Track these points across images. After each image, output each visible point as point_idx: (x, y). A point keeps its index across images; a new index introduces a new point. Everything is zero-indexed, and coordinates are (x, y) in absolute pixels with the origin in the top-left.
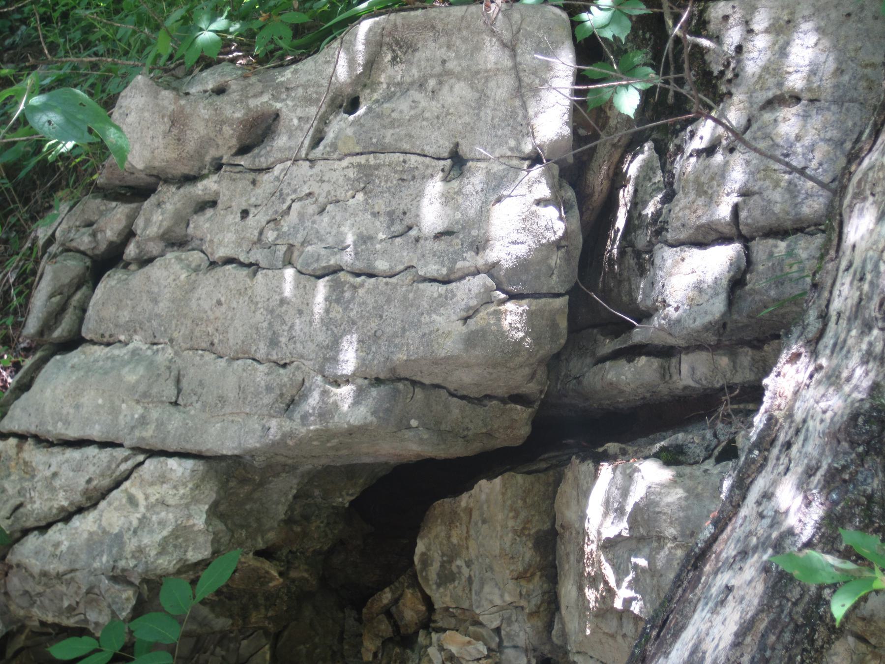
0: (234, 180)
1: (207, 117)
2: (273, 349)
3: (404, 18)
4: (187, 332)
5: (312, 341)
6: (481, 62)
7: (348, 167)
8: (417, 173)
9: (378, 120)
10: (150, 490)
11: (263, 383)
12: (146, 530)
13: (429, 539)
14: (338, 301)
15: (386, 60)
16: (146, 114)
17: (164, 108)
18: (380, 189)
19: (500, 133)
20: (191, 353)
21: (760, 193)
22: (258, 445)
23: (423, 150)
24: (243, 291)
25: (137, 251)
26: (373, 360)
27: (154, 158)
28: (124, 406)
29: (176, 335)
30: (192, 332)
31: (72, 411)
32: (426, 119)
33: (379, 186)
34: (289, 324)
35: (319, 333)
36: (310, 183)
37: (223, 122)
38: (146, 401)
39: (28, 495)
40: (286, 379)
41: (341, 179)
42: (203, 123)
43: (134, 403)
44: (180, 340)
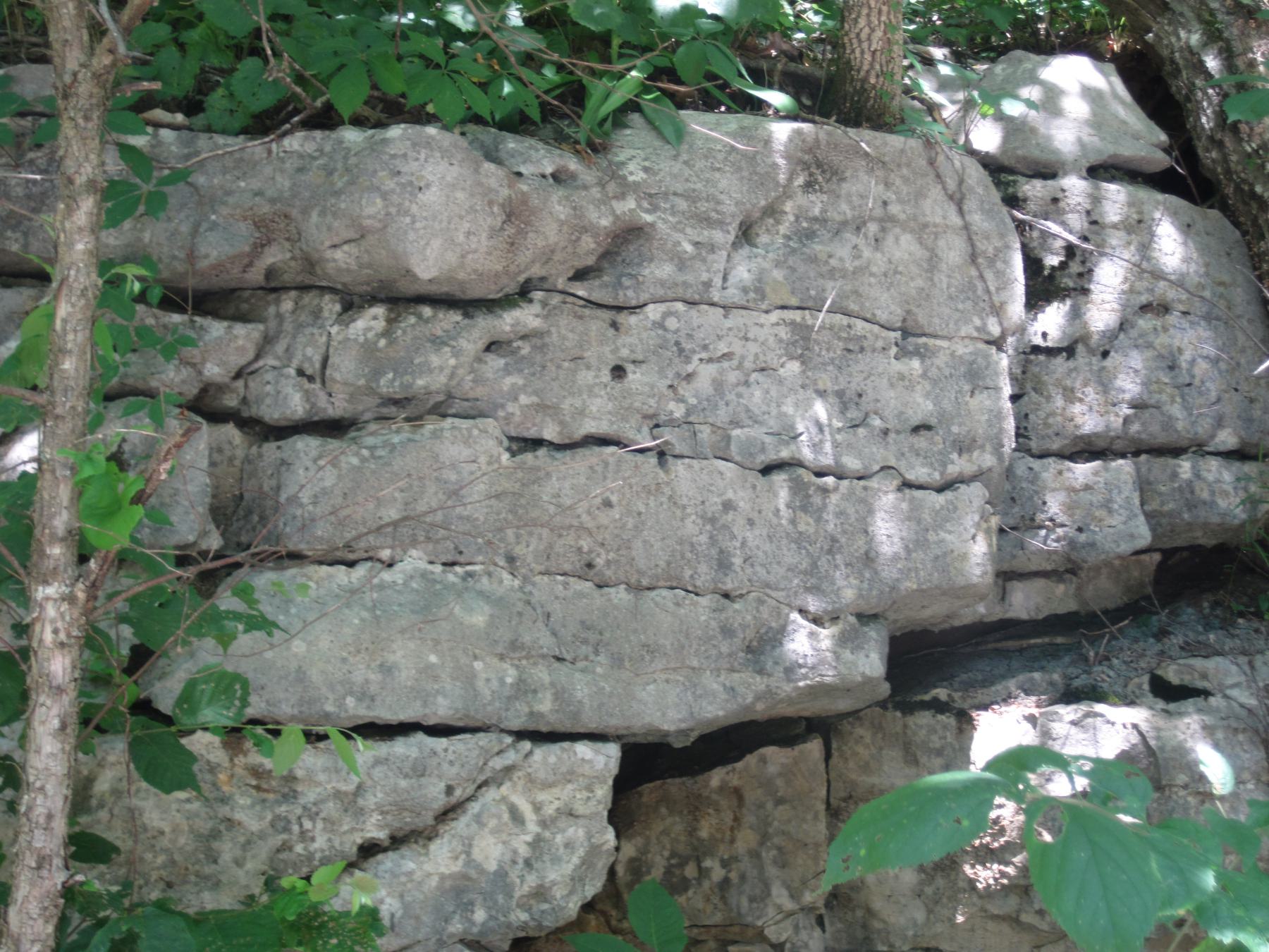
0: (581, 317)
1: (562, 217)
2: (726, 575)
3: (829, 134)
4: (542, 547)
5: (779, 563)
6: (928, 213)
7: (778, 324)
8: (865, 344)
9: (813, 266)
10: (542, 796)
11: (713, 624)
12: (546, 858)
13: (648, 838)
14: (804, 509)
15: (796, 184)
16: (460, 195)
17: (490, 190)
18: (820, 360)
19: (960, 306)
20: (546, 578)
21: (1157, 407)
22: (721, 713)
23: (874, 315)
24: (653, 487)
25: (308, 407)
26: (871, 589)
27: (462, 266)
28: (478, 665)
29: (519, 550)
30: (551, 546)
31: (374, 677)
32: (872, 275)
33: (819, 355)
34: (740, 538)
35: (785, 552)
36: (729, 339)
37: (585, 230)
38: (517, 655)
39: (296, 828)
40: (749, 617)
41: (772, 339)
42: (555, 226)
43: (495, 661)
44: (530, 559)
